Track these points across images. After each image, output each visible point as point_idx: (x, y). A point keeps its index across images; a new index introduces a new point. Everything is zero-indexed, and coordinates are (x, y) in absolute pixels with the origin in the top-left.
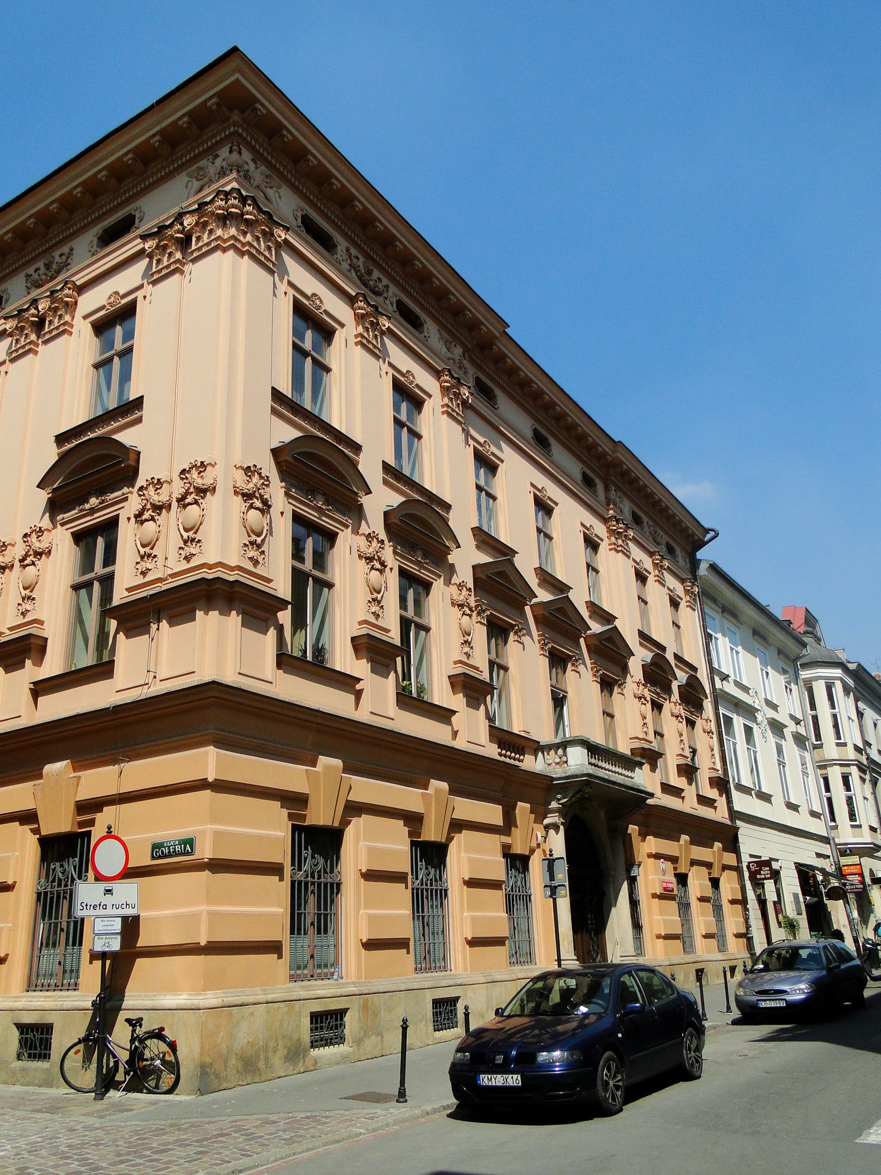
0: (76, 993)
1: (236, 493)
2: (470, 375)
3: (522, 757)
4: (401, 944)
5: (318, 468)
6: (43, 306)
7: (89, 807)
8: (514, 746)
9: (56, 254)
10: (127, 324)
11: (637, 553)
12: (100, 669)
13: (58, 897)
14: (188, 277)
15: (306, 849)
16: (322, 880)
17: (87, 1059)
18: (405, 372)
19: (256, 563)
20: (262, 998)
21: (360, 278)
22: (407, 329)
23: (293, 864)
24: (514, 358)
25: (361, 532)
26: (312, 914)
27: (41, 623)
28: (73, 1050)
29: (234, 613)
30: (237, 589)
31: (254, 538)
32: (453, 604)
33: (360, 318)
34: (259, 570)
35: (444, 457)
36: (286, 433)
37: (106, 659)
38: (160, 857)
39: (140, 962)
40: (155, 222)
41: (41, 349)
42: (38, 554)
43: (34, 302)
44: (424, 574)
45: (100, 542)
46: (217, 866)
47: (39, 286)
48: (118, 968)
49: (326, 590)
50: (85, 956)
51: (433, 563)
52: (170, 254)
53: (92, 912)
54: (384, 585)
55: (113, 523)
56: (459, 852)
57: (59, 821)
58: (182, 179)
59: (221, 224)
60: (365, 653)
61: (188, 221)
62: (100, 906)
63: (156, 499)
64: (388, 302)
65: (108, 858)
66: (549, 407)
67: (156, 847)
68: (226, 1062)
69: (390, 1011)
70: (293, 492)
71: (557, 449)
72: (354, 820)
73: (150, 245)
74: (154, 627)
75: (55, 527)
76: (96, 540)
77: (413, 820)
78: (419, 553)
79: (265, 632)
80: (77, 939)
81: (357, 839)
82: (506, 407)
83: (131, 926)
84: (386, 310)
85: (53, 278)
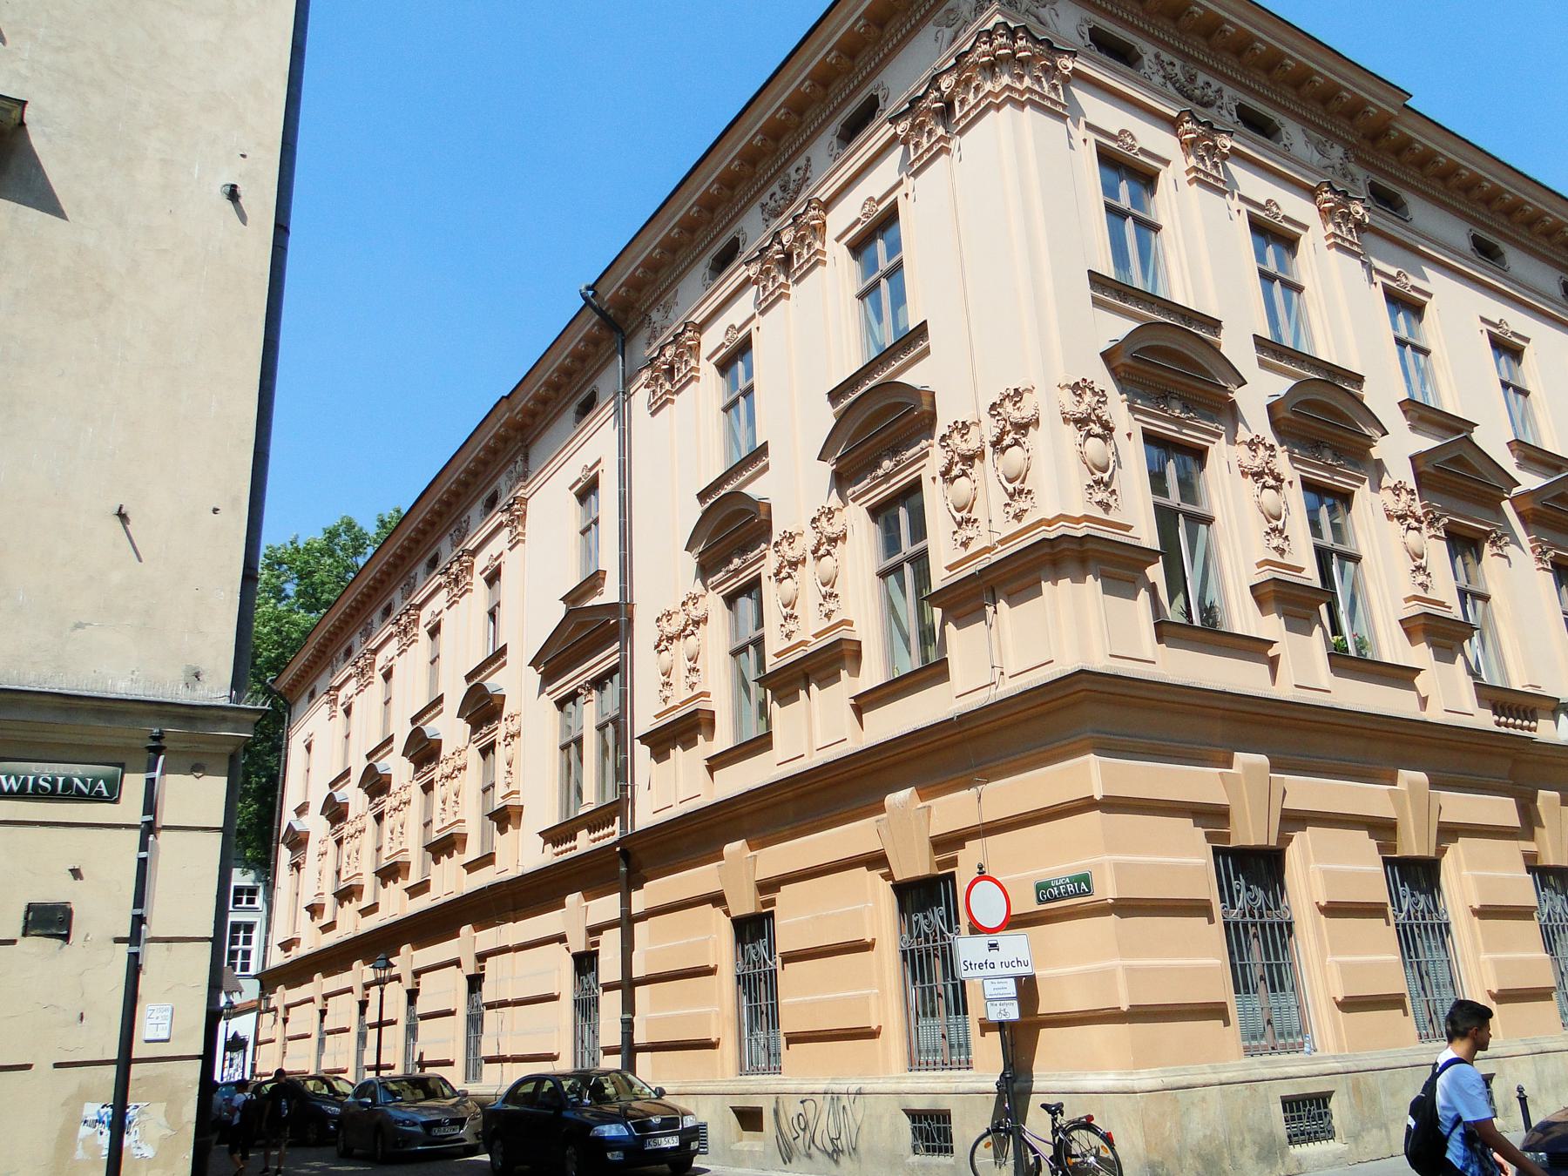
0: (970, 1072)
1: (1066, 420)
2: (1360, 183)
3: (1533, 724)
4: (1393, 1002)
5: (1169, 367)
6: (787, 237)
7: (948, 843)
8: (1510, 709)
9: (792, 170)
10: (889, 234)
11: (1098, 110)
12: (928, 673)
13: (928, 955)
14: (956, 156)
15: (1237, 878)
16: (1266, 919)
17: (999, 1155)
18: (1116, 133)
19: (1106, 507)
20: (1214, 1078)
21: (1180, 90)
22: (1254, 141)
23: (1223, 901)
24: (1425, 140)
25: (1239, 439)
26: (1259, 966)
27: (850, 623)
28: (982, 1143)
29: (1090, 578)
30: (1089, 546)
31: (1099, 475)
32: (1389, 517)
33: (1189, 146)
34: (1112, 516)
35: (1341, 311)
36: (1118, 327)
37: (933, 659)
38: (1048, 901)
39: (1044, 1034)
40: (905, 96)
41: (793, 290)
42: (833, 541)
43: (777, 234)
44: (1340, 482)
45: (903, 513)
46: (1126, 908)
47: (778, 215)
48: (1019, 1040)
49: (1203, 527)
50: (974, 1028)
51: (1350, 463)
52: (930, 133)
53: (978, 972)
54: (1112, 459)
55: (915, 487)
56: (1458, 870)
57: (915, 864)
58: (929, 30)
59: (988, 75)
60: (1273, 605)
61: (946, 83)
62: (988, 968)
63: (964, 448)
64: (1224, 112)
65: (987, 905)
66: (1491, 198)
67: (1041, 888)
68: (1179, 1160)
69: (1393, 1095)
70: (1139, 404)
71: (1514, 258)
72: (1297, 835)
73: (903, 127)
74: (990, 610)
75: (846, 504)
76: (899, 511)
77: (1382, 829)
78: (1327, 453)
79: (1134, 597)
80: (960, 1004)
81: (1306, 862)
82: (1422, 213)
83: (1027, 989)
84: (1222, 124)
85: (792, 201)
